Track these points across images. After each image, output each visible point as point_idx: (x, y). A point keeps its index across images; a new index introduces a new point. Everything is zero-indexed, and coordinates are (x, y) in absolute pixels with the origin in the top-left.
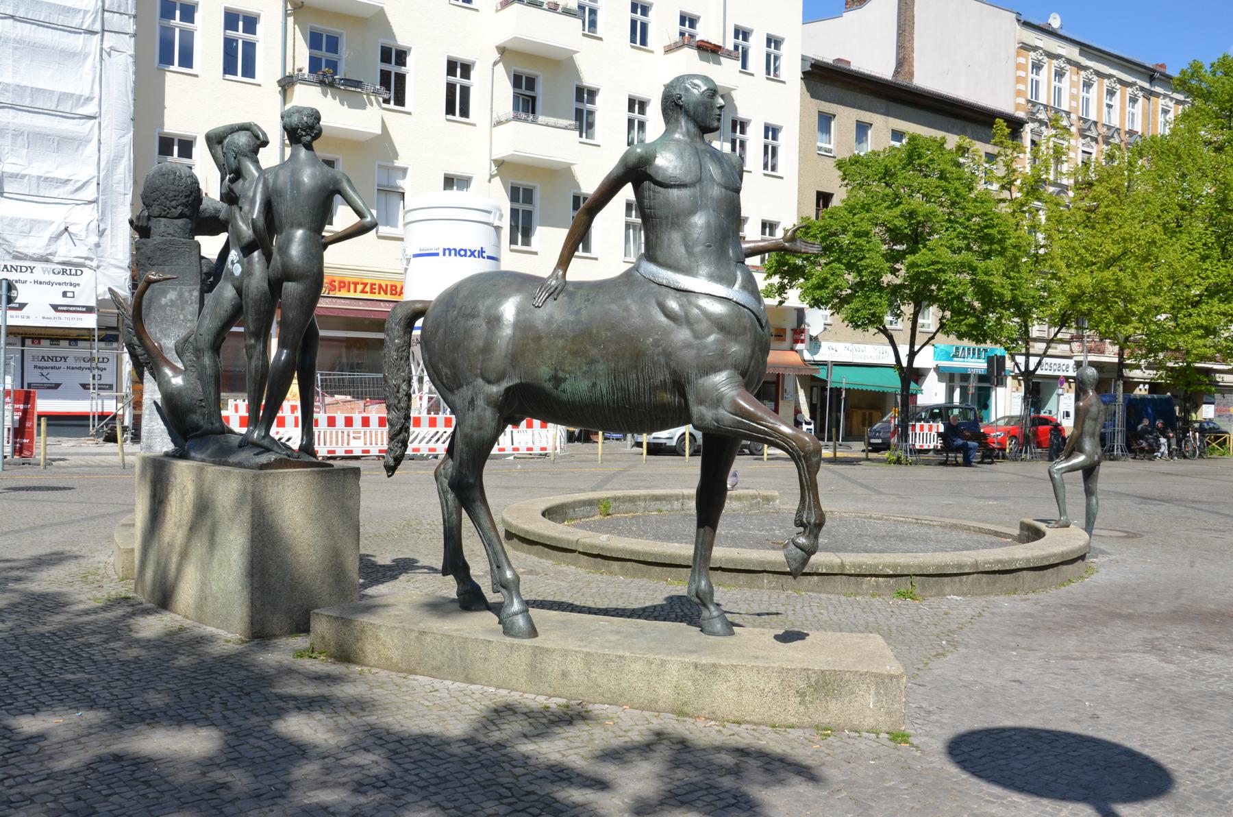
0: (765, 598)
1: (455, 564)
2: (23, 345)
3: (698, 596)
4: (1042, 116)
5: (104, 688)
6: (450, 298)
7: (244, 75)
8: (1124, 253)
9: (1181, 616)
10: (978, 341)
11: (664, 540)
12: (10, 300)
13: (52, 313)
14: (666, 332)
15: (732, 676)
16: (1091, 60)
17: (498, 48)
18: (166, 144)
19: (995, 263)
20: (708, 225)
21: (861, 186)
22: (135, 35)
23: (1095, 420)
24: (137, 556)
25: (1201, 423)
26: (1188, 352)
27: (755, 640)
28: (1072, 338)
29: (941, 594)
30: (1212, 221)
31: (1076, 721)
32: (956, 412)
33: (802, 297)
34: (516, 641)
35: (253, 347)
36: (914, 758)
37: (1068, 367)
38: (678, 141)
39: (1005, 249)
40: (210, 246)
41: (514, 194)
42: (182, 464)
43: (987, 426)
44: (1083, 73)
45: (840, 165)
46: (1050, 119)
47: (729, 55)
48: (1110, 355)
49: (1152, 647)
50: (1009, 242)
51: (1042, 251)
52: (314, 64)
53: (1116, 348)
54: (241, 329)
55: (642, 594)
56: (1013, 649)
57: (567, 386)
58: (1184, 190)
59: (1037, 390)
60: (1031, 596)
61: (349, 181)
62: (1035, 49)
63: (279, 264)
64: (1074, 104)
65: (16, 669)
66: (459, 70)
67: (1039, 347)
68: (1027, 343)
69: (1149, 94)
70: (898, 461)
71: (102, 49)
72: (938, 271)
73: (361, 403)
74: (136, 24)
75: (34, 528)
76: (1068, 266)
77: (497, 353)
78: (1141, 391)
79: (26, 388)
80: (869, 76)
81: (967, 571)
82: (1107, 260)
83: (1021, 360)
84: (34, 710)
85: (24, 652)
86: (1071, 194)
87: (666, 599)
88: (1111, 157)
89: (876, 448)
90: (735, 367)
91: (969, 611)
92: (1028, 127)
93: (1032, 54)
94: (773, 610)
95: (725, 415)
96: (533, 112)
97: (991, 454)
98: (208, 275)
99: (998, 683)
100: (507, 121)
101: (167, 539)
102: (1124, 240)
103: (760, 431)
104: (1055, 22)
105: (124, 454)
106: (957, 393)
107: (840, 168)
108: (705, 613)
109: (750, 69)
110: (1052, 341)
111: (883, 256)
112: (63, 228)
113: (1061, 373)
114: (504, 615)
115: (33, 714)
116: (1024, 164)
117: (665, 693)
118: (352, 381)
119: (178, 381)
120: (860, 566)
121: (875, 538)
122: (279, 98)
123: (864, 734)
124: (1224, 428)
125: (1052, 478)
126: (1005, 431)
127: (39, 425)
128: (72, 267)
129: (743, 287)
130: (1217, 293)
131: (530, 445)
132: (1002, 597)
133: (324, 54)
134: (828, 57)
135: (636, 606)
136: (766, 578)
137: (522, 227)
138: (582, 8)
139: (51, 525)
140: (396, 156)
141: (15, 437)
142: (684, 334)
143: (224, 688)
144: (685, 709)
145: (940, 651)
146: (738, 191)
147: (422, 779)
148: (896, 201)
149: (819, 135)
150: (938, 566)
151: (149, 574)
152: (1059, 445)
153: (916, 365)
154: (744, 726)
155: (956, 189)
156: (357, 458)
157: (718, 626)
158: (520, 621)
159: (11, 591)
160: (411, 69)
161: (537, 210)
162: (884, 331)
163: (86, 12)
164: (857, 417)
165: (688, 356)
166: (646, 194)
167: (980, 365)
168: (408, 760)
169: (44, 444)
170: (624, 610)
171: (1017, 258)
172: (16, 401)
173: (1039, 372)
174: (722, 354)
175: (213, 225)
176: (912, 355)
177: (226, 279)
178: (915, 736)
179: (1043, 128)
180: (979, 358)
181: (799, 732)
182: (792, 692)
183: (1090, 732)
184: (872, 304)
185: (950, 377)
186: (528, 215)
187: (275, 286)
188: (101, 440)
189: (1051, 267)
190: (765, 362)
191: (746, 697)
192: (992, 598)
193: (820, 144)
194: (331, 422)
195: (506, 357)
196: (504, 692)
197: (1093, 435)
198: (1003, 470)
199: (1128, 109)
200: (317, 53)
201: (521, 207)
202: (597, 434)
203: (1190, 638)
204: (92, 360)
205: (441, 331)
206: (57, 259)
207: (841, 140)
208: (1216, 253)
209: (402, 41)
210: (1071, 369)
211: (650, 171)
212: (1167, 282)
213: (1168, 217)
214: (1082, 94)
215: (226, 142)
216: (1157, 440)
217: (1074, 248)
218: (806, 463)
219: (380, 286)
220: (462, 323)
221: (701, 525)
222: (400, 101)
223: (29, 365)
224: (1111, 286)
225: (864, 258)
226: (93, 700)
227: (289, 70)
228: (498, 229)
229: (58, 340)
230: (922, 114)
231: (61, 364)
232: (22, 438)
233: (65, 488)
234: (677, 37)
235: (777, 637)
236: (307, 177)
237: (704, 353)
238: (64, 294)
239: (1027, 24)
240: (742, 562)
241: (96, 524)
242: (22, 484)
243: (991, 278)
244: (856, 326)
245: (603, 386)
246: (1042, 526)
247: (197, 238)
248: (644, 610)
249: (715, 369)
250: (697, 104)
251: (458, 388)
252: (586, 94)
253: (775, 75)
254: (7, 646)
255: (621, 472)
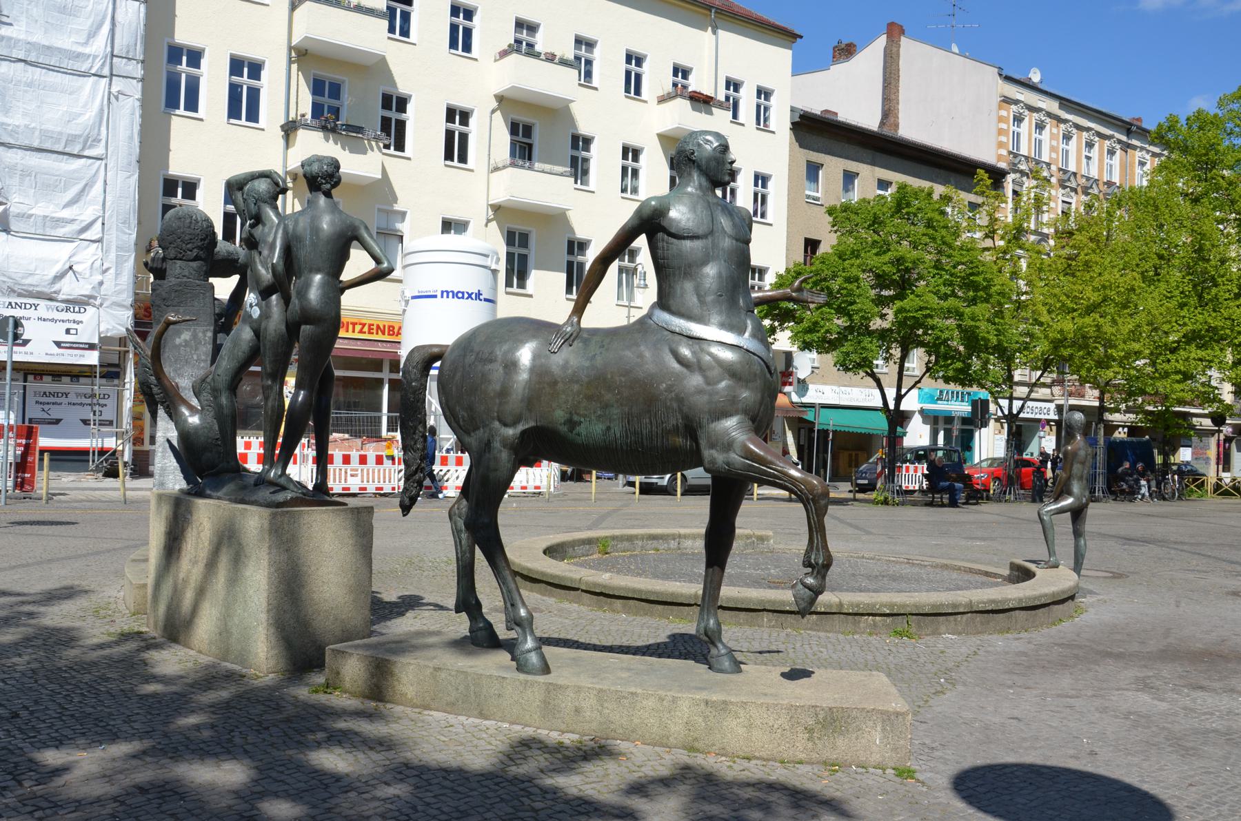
0: (766, 636)
1: (468, 603)
2: (25, 381)
3: (706, 634)
4: (1023, 167)
5: (125, 722)
6: (467, 343)
7: (248, 119)
8: (1104, 300)
9: (1169, 655)
10: (963, 385)
11: (662, 579)
12: (16, 337)
13: (56, 350)
14: (679, 378)
15: (742, 713)
16: (1070, 113)
17: (496, 96)
18: (170, 186)
19: (982, 310)
20: (720, 275)
21: (850, 232)
22: (142, 80)
23: (1083, 463)
24: (150, 590)
25: (1179, 465)
26: (1166, 397)
27: (762, 678)
28: (1053, 382)
29: (936, 633)
30: (1189, 269)
31: (1076, 758)
32: (940, 454)
33: (793, 339)
34: (530, 677)
35: (270, 387)
36: (921, 793)
37: (1049, 410)
38: (690, 194)
39: (990, 296)
40: (224, 287)
41: (510, 237)
42: (201, 502)
43: (971, 467)
44: (1062, 126)
45: (831, 212)
46: (1031, 170)
47: (720, 105)
48: (1091, 399)
49: (1144, 685)
50: (994, 289)
51: (1023, 298)
52: (317, 110)
53: (1096, 393)
54: (258, 369)
55: (645, 632)
56: (1010, 687)
57: (582, 429)
58: (1162, 240)
59: (1019, 431)
60: (1024, 635)
61: (366, 228)
62: (1016, 102)
63: (297, 308)
64: (1054, 155)
65: (36, 702)
66: (457, 118)
67: (1021, 391)
68: (1011, 387)
69: (1126, 147)
70: (885, 502)
71: (110, 93)
72: (926, 316)
73: (359, 441)
74: (144, 68)
75: (41, 563)
76: (1049, 312)
77: (514, 396)
78: (1121, 434)
79: (27, 424)
80: (856, 127)
81: (961, 610)
82: (1088, 307)
83: (1004, 403)
84: (59, 743)
85: (43, 686)
86: (1052, 242)
87: (669, 637)
88: (1089, 207)
89: (863, 489)
90: (745, 412)
91: (964, 650)
92: (1010, 178)
93: (1013, 107)
94: (774, 648)
95: (736, 458)
96: (530, 159)
97: (977, 495)
98: (219, 316)
99: (997, 720)
100: (505, 167)
101: (182, 575)
102: (1104, 287)
103: (770, 475)
104: (1036, 77)
105: (125, 489)
106: (941, 436)
107: (830, 214)
108: (714, 651)
109: (741, 120)
110: (1035, 385)
111: (873, 301)
112: (67, 266)
113: (1042, 417)
114: (518, 652)
115: (57, 747)
116: (1006, 214)
117: (676, 728)
118: (349, 420)
119: (194, 420)
120: (858, 606)
121: (869, 577)
122: (282, 142)
123: (871, 770)
124: (1201, 471)
125: (1041, 520)
126: (988, 473)
127: (41, 460)
128: (79, 303)
129: (753, 336)
130: (1193, 339)
131: (524, 484)
132: (995, 636)
133: (326, 100)
134: (816, 108)
135: (640, 643)
136: (766, 617)
137: (518, 271)
138: (578, 58)
139: (58, 560)
140: (395, 200)
141: (17, 471)
142: (696, 380)
143: (244, 723)
144: (696, 744)
145: (939, 689)
146: (748, 242)
147: (443, 813)
148: (884, 248)
149: (807, 183)
150: (933, 606)
151: (162, 609)
152: (1041, 486)
153: (902, 408)
154: (754, 762)
155: (943, 237)
156: (354, 495)
157: (726, 664)
158: (534, 658)
159: (25, 625)
160: (411, 115)
161: (533, 253)
162: (873, 375)
163: (95, 57)
164: (844, 457)
165: (701, 401)
166: (660, 244)
167: (964, 408)
168: (429, 794)
169: (45, 479)
170: (628, 647)
171: (1000, 304)
172: (18, 436)
173: (1022, 415)
174: (733, 400)
175: (225, 267)
176: (899, 398)
177: (244, 321)
178: (920, 772)
179: (1025, 179)
180: (962, 401)
181: (808, 768)
182: (800, 729)
183: (1090, 769)
184: (863, 348)
185: (933, 419)
186: (524, 259)
187: (292, 329)
188: (100, 475)
189: (1033, 312)
190: (773, 408)
191: (756, 734)
192: (986, 637)
193: (808, 192)
194: (346, 460)
195: (522, 401)
196: (518, 728)
197: (1081, 478)
198: (987, 511)
199: (1107, 161)
200: (320, 99)
201: (517, 251)
202: (590, 473)
203: (1180, 677)
204: (93, 396)
205: (459, 374)
206: (61, 297)
207: (828, 188)
208: (1193, 301)
209: (403, 88)
210: (1052, 412)
211: (664, 223)
212: (1146, 328)
213: (1147, 266)
214: (1062, 146)
215: (246, 188)
216: (1137, 481)
217: (1055, 295)
218: (816, 507)
219: (378, 327)
220: (480, 367)
221: (709, 564)
222: (400, 146)
223: (30, 400)
224: (1091, 331)
225: (854, 303)
226: (115, 734)
227: (292, 116)
228: (495, 272)
229: (60, 376)
230: (893, 160)
231: (63, 400)
232: (24, 472)
233: (68, 523)
234: (670, 88)
235: (784, 675)
236: (326, 224)
237: (716, 398)
238: (68, 331)
239: (1008, 79)
240: (743, 600)
241: (108, 556)
242: (26, 519)
243: (978, 324)
244: (847, 369)
245: (617, 430)
246: (1032, 567)
247: (211, 280)
248: (648, 647)
249: (726, 414)
250: (709, 160)
251: (474, 430)
252: (581, 142)
253: (765, 125)
254: (26, 680)
255: (614, 511)
